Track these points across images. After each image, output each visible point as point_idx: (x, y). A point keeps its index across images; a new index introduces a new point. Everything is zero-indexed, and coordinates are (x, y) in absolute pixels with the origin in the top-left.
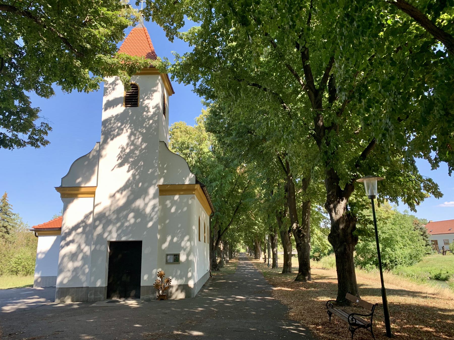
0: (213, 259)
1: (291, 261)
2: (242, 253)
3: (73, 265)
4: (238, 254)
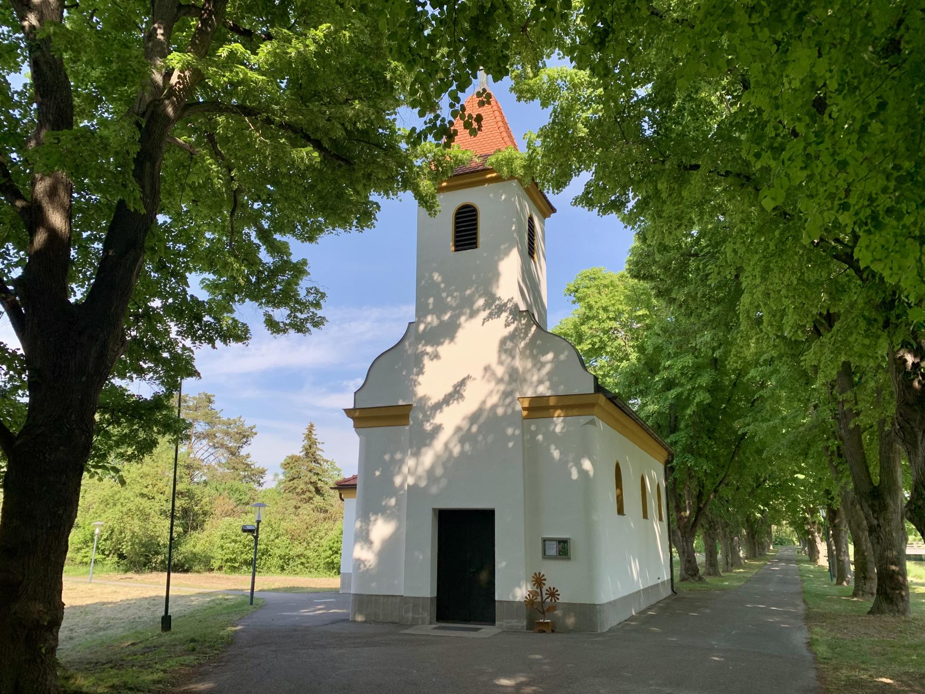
3: (373, 552)
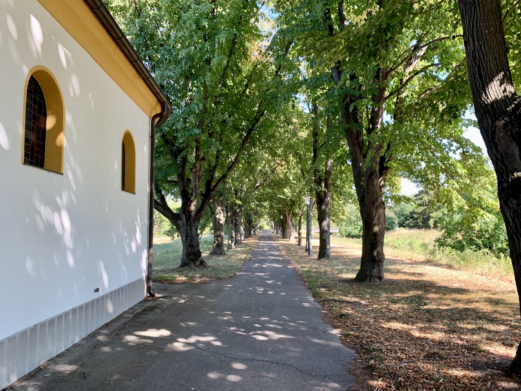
0: (191, 241)
1: (382, 250)
2: (266, 230)
4: (261, 232)
